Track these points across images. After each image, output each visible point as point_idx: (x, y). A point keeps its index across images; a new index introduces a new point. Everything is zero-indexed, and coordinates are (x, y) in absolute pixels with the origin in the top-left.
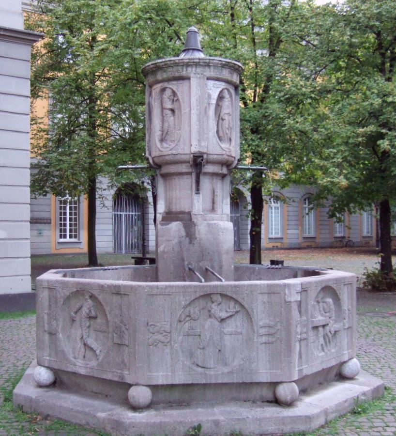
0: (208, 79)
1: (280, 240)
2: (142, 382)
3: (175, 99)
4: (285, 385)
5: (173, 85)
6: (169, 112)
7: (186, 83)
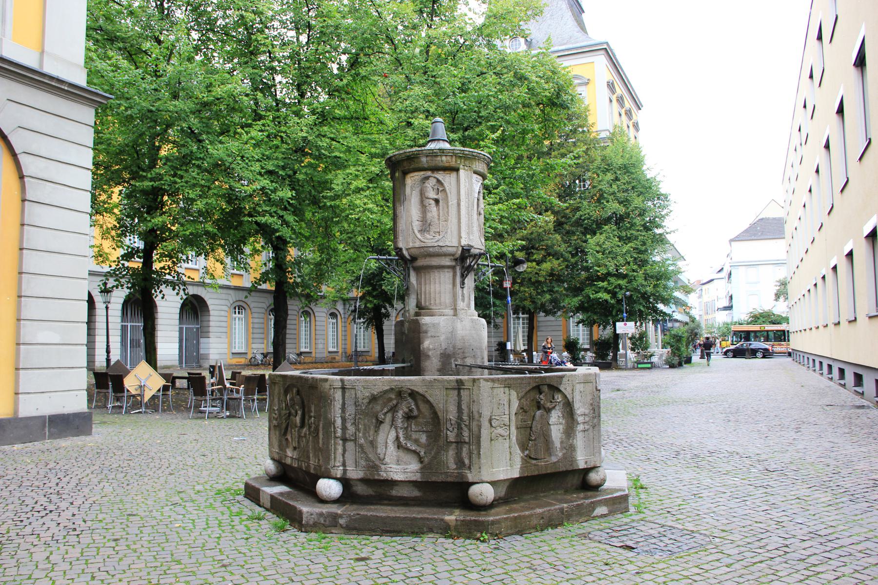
0: (475, 172)
1: (245, 356)
2: (485, 479)
3: (441, 189)
4: (477, 485)
5: (440, 176)
6: (433, 202)
7: (454, 174)
